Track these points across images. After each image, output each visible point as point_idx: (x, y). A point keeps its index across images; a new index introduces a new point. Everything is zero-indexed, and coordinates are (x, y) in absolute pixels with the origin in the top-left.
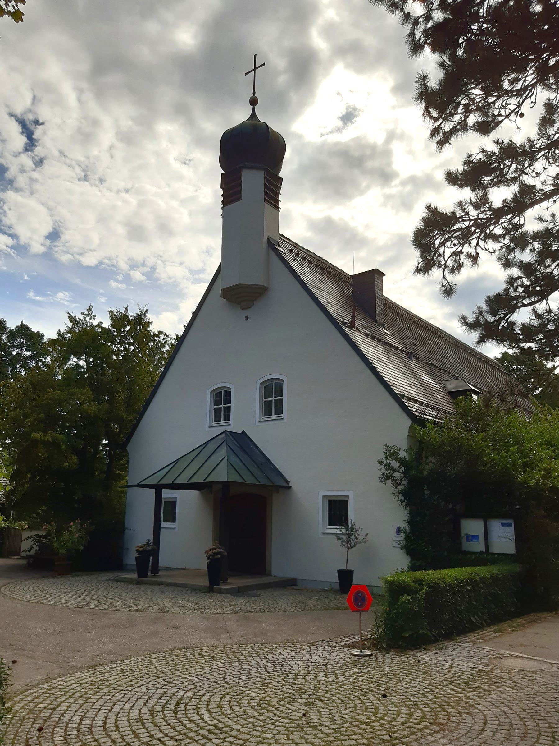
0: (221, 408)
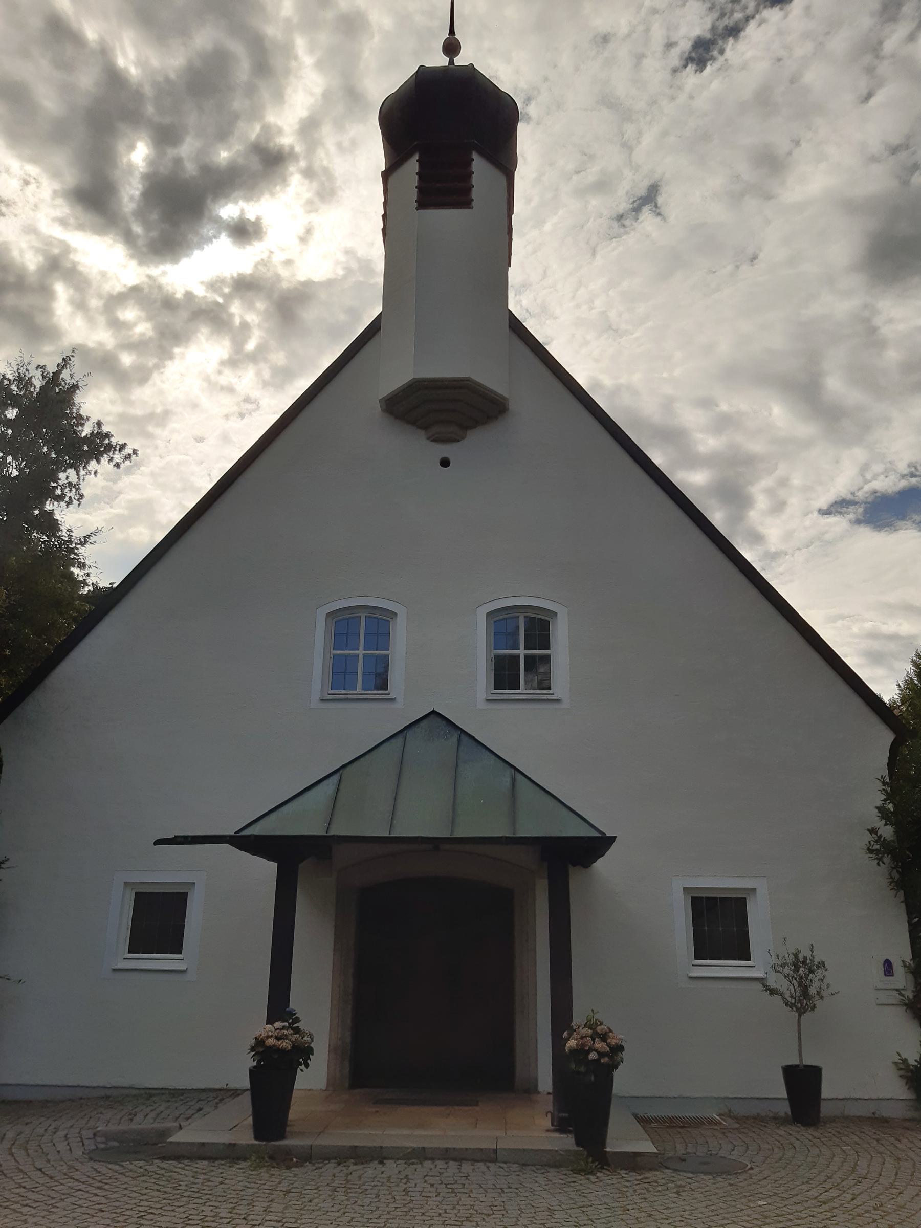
0: (357, 656)
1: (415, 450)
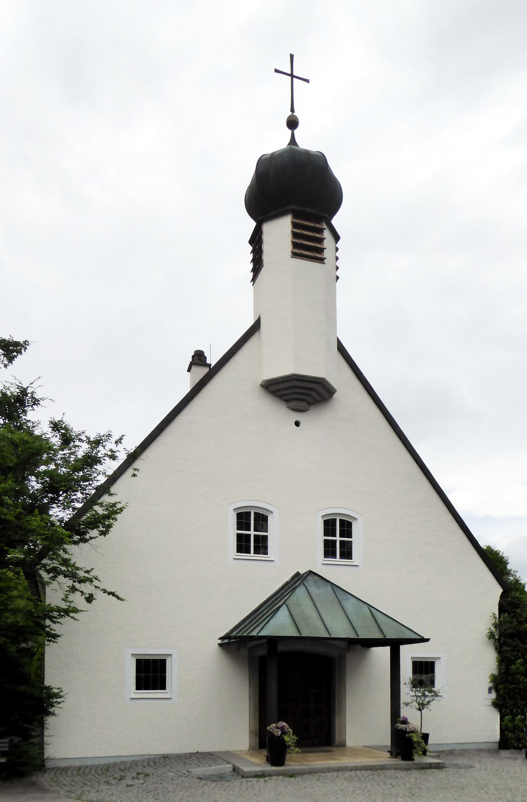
1: (277, 416)
